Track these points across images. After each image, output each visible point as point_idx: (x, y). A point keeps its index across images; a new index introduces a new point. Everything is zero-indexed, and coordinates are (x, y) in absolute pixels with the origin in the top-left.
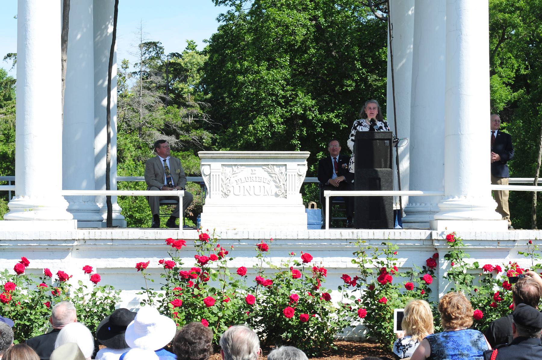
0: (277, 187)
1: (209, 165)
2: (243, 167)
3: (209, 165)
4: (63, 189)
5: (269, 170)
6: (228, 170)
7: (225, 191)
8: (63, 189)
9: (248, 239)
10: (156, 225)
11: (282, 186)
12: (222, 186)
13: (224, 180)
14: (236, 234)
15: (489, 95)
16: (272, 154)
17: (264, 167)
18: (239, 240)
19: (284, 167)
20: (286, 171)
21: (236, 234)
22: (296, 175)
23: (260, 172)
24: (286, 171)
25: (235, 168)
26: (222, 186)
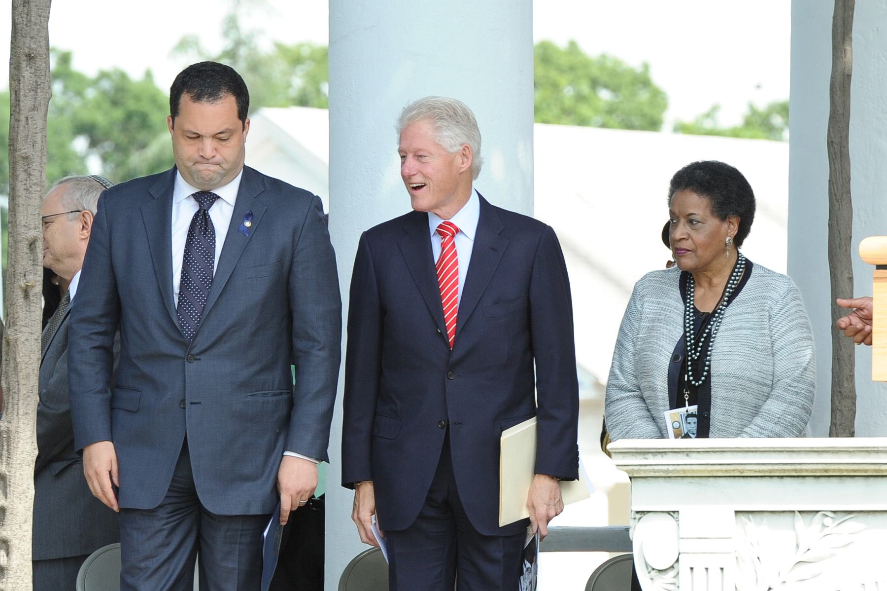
1: (672, 513)
2: (853, 525)
3: (672, 513)
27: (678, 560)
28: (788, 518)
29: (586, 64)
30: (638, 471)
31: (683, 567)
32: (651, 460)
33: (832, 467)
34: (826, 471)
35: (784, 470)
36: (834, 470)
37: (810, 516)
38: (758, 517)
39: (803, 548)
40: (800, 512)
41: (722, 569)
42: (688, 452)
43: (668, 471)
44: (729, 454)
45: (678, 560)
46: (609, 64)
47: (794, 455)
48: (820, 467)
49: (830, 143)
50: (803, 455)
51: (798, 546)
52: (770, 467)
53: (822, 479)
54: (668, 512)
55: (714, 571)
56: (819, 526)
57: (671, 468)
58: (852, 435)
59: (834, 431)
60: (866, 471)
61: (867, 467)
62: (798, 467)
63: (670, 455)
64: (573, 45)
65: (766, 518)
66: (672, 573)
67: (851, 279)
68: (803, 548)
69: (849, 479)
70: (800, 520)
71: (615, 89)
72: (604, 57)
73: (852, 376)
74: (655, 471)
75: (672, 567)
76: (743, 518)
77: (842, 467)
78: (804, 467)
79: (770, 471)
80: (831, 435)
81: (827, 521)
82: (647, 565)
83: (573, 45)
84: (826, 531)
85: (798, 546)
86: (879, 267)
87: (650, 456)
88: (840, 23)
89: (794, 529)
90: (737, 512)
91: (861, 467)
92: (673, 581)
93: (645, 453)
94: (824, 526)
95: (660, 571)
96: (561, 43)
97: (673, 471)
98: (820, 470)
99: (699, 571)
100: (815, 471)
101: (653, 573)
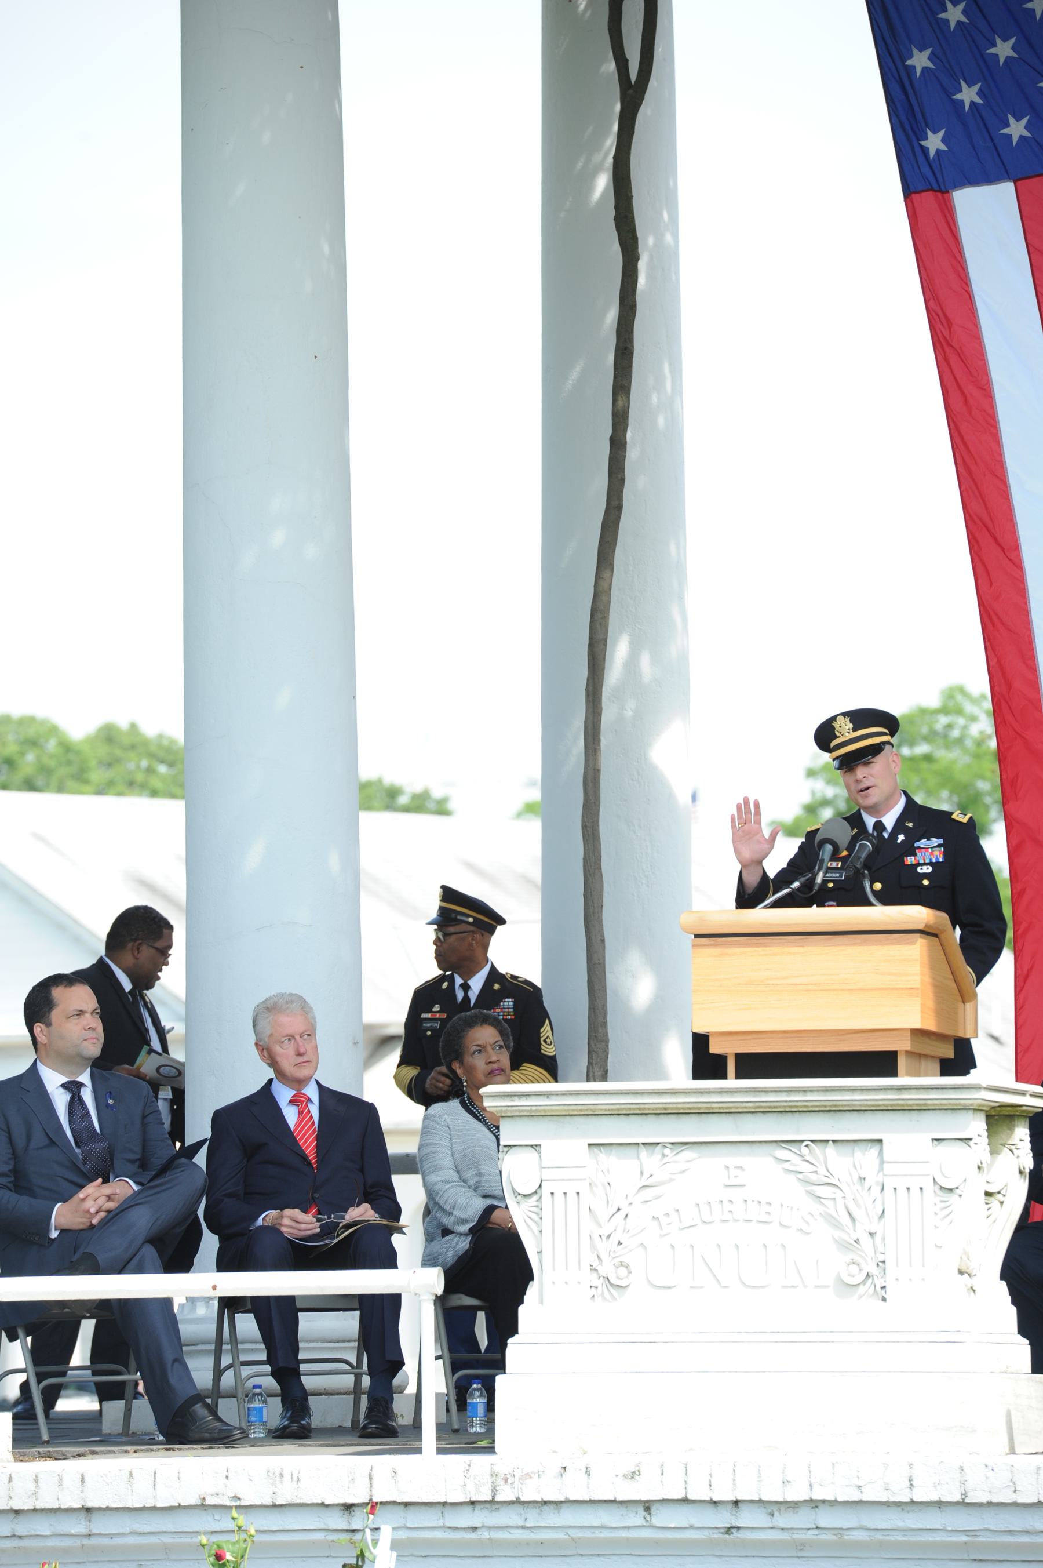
0: (844, 1246)
1: (536, 1147)
2: (688, 1154)
3: (536, 1147)
4: (394, 1266)
5: (805, 1167)
6: (622, 1169)
7: (607, 1268)
8: (394, 1266)
9: (685, 1501)
10: (296, 1427)
11: (866, 1241)
12: (593, 1247)
13: (603, 1214)
14: (633, 1475)
15: (109, 802)
16: (853, 1090)
17: (782, 1153)
18: (647, 1506)
19: (873, 1151)
20: (881, 1169)
21: (633, 1475)
22: (929, 1187)
23: (762, 1171)
24: (881, 1169)
25: (650, 1160)
26: (593, 1247)
27: (540, 1186)
28: (632, 1151)
29: (146, 743)
30: (506, 1111)
31: (545, 1192)
32: (517, 1102)
33: (671, 1106)
34: (665, 1109)
35: (630, 1109)
36: (672, 1109)
37: (651, 1148)
38: (608, 1148)
39: (646, 1175)
40: (643, 1144)
41: (908, 1189)
42: (548, 1095)
43: (531, 1111)
44: (584, 1096)
45: (540, 1186)
46: (165, 743)
47: (638, 1096)
48: (660, 1106)
49: (584, 827)
50: (646, 1096)
51: (642, 1173)
52: (579, 1107)
53: (662, 1116)
54: (532, 1146)
55: (572, 1196)
56: (660, 1156)
57: (534, 1108)
58: (604, 1078)
59: (591, 1074)
60: (699, 1108)
61: (700, 1105)
62: (642, 1106)
63: (533, 1098)
64: (133, 726)
65: (614, 1149)
66: (535, 1198)
67: (603, 941)
68: (646, 1175)
69: (685, 1116)
70: (643, 1153)
71: (171, 765)
72: (161, 736)
73: (605, 1023)
74: (520, 1111)
75: (536, 1192)
76: (595, 1150)
77: (680, 1106)
78: (647, 1106)
79: (618, 1110)
80: (588, 1080)
81: (667, 1151)
82: (514, 1191)
83: (133, 726)
84: (666, 1160)
85: (642, 1173)
86: (697, 936)
87: (516, 1098)
88: (590, 726)
89: (638, 1158)
90: (589, 1145)
91: (695, 1105)
92: (536, 1204)
93: (511, 1096)
94: (664, 1155)
95: (941, 1188)
96: (123, 724)
97: (536, 1111)
98: (660, 1109)
99: (558, 1196)
100: (657, 1109)
101: (519, 1197)
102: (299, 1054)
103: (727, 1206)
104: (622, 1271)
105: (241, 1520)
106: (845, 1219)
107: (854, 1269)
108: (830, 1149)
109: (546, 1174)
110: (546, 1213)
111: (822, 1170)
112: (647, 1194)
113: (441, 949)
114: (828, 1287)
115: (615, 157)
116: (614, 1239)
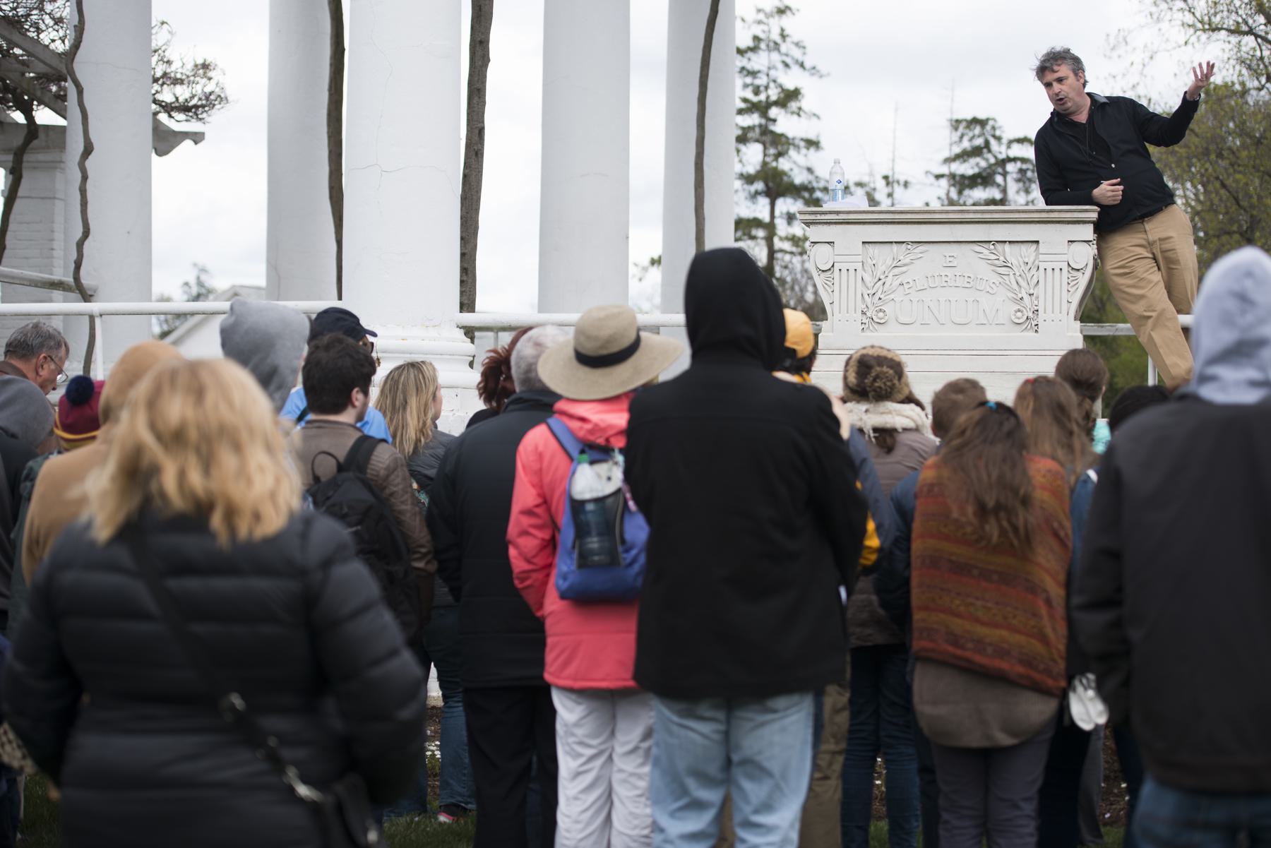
0: (1015, 301)
6: (884, 256)
11: (1026, 298)
17: (977, 248)
22: (1065, 266)
55: (852, 271)
99: (844, 271)
102: (1206, 152)
103: (945, 279)
104: (881, 314)
105: (962, 609)
106: (1015, 286)
107: (1019, 314)
108: (1007, 246)
109: (837, 259)
110: (836, 281)
111: (1002, 258)
112: (896, 271)
113: (1060, 109)
114: (340, 298)
115: (344, 50)
116: (877, 297)
